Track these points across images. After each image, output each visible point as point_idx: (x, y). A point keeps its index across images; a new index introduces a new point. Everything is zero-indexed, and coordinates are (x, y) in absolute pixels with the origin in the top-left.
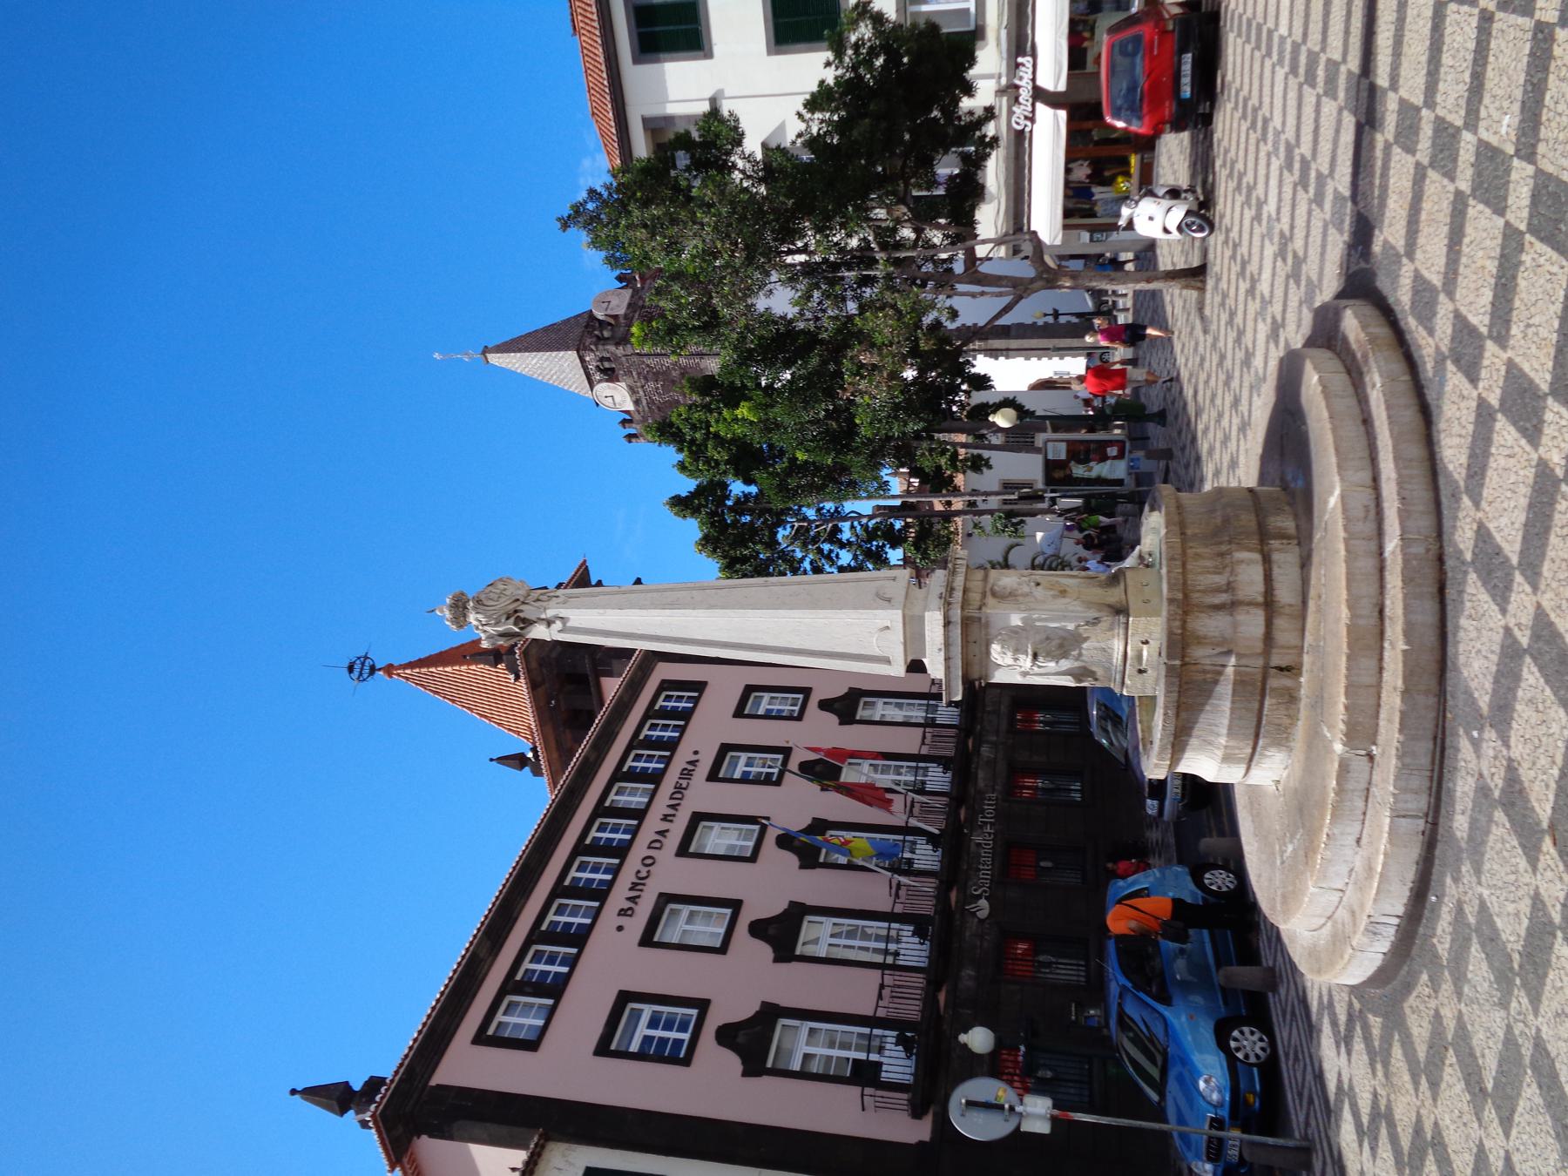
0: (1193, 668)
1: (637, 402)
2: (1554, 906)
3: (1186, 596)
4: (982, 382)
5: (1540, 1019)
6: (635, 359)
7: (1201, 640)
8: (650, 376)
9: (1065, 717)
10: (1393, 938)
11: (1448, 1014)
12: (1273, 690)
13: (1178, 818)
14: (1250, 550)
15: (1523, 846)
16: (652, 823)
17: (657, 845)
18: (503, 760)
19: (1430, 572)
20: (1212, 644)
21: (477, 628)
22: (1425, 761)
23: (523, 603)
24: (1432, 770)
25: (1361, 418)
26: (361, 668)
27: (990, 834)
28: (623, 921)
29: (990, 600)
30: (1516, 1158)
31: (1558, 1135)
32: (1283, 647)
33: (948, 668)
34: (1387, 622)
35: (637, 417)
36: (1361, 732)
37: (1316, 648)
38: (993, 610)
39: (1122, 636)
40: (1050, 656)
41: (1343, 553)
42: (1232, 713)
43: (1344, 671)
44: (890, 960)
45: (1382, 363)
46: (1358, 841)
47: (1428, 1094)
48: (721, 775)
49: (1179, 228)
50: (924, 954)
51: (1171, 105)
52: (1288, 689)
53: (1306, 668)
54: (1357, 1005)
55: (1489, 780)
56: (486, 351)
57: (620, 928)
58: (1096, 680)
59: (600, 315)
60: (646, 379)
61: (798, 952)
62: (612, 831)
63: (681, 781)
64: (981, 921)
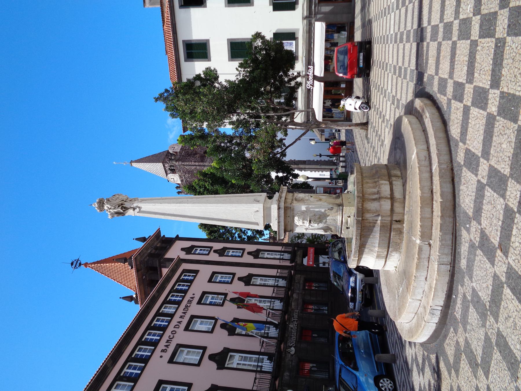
0: (366, 221)
1: (182, 181)
2: (502, 275)
3: (363, 195)
4: (296, 176)
5: (499, 324)
6: (182, 166)
7: (368, 211)
8: (187, 172)
9: (321, 285)
10: (439, 316)
11: (461, 341)
12: (394, 229)
13: (361, 309)
14: (386, 180)
15: (488, 259)
16: (176, 319)
17: (177, 327)
18: (124, 298)
19: (449, 174)
20: (373, 212)
21: (107, 211)
22: (450, 242)
23: (125, 201)
24: (452, 246)
25: (422, 130)
26: (76, 264)
27: (296, 324)
28: (163, 354)
29: (294, 202)
30: (491, 387)
31: (509, 369)
32: (397, 213)
33: (279, 226)
34: (434, 194)
35: (181, 186)
36: (426, 235)
37: (409, 211)
38: (295, 204)
39: (341, 214)
40: (315, 221)
41: (418, 171)
42: (380, 238)
43: (419, 212)
44: (259, 369)
45: (429, 110)
46: (426, 279)
47: (455, 376)
48: (202, 302)
49: (359, 108)
50: (271, 366)
51: (356, 69)
52: (399, 229)
53: (405, 220)
54: (426, 354)
55: (474, 241)
56: (132, 162)
57: (161, 357)
58: (332, 231)
59: (171, 152)
60: (185, 173)
61: (226, 366)
62: (161, 322)
63: (187, 304)
64: (292, 355)
